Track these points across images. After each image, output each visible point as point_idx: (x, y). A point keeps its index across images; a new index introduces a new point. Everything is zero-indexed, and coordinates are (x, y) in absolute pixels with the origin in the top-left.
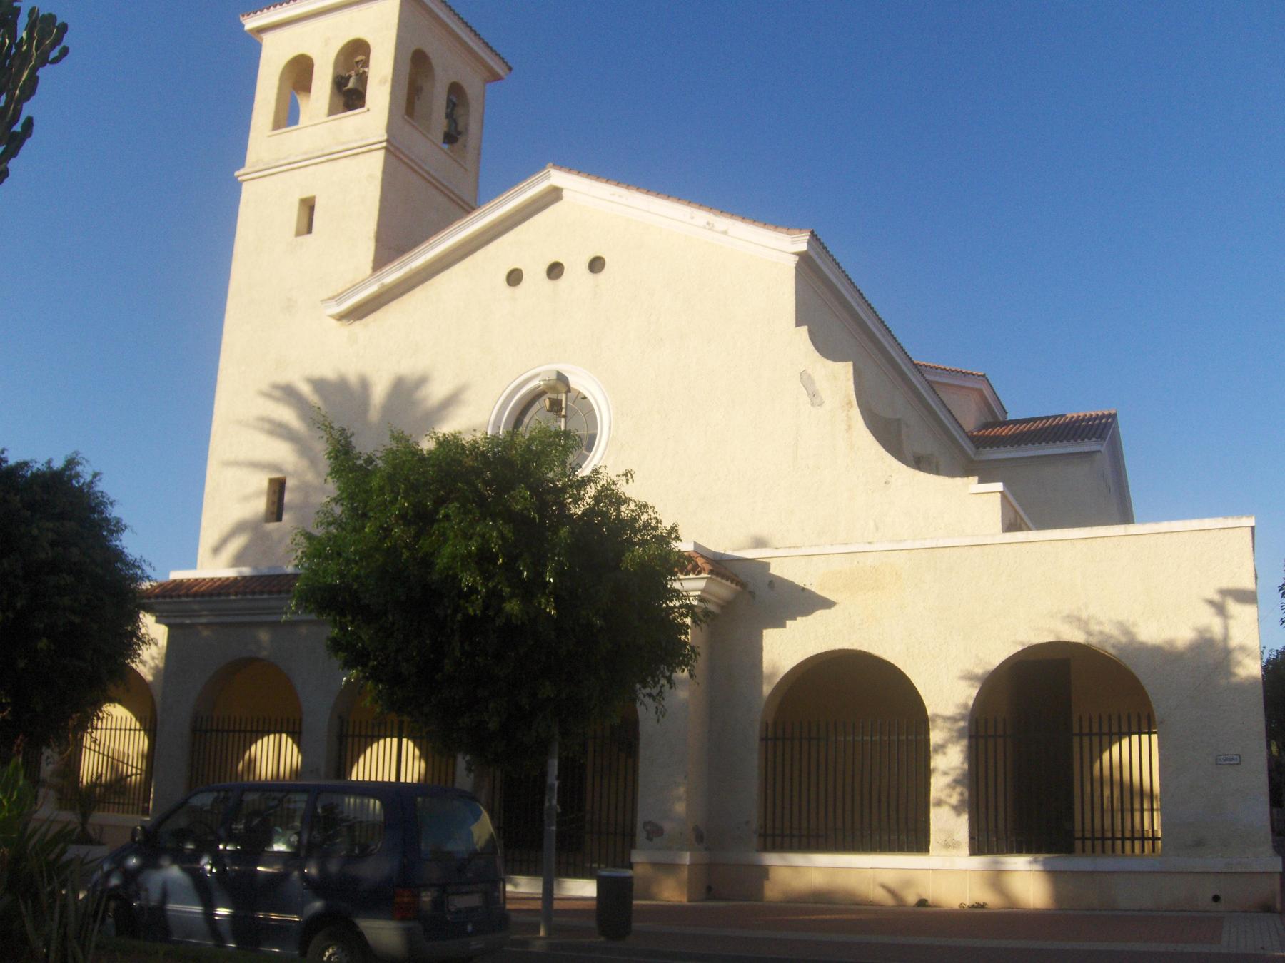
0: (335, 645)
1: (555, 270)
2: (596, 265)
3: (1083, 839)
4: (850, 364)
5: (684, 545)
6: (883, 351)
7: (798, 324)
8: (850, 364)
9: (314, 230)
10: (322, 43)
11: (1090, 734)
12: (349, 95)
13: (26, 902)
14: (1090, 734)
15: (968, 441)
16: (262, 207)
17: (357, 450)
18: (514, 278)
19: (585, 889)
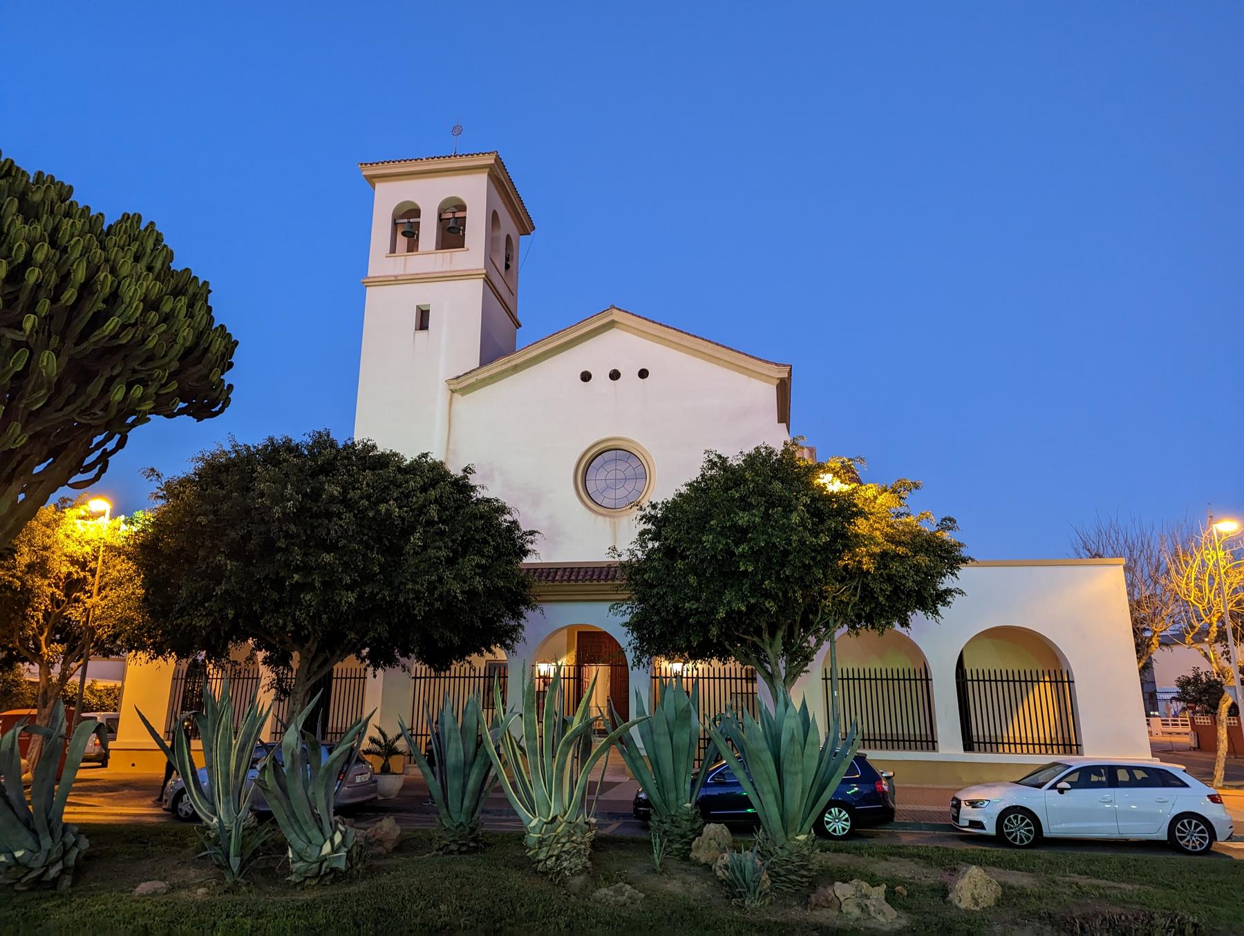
0: (374, 447)
1: (615, 375)
2: (643, 374)
3: (979, 743)
4: (1166, 838)
5: (541, 554)
6: (512, 203)
7: (779, 422)
8: (1166, 838)
9: (521, 322)
10: (428, 196)
11: (1038, 681)
12: (452, 233)
13: (158, 815)
14: (1038, 681)
15: (485, 368)
16: (385, 311)
17: (529, 614)
18: (586, 377)
19: (543, 668)
